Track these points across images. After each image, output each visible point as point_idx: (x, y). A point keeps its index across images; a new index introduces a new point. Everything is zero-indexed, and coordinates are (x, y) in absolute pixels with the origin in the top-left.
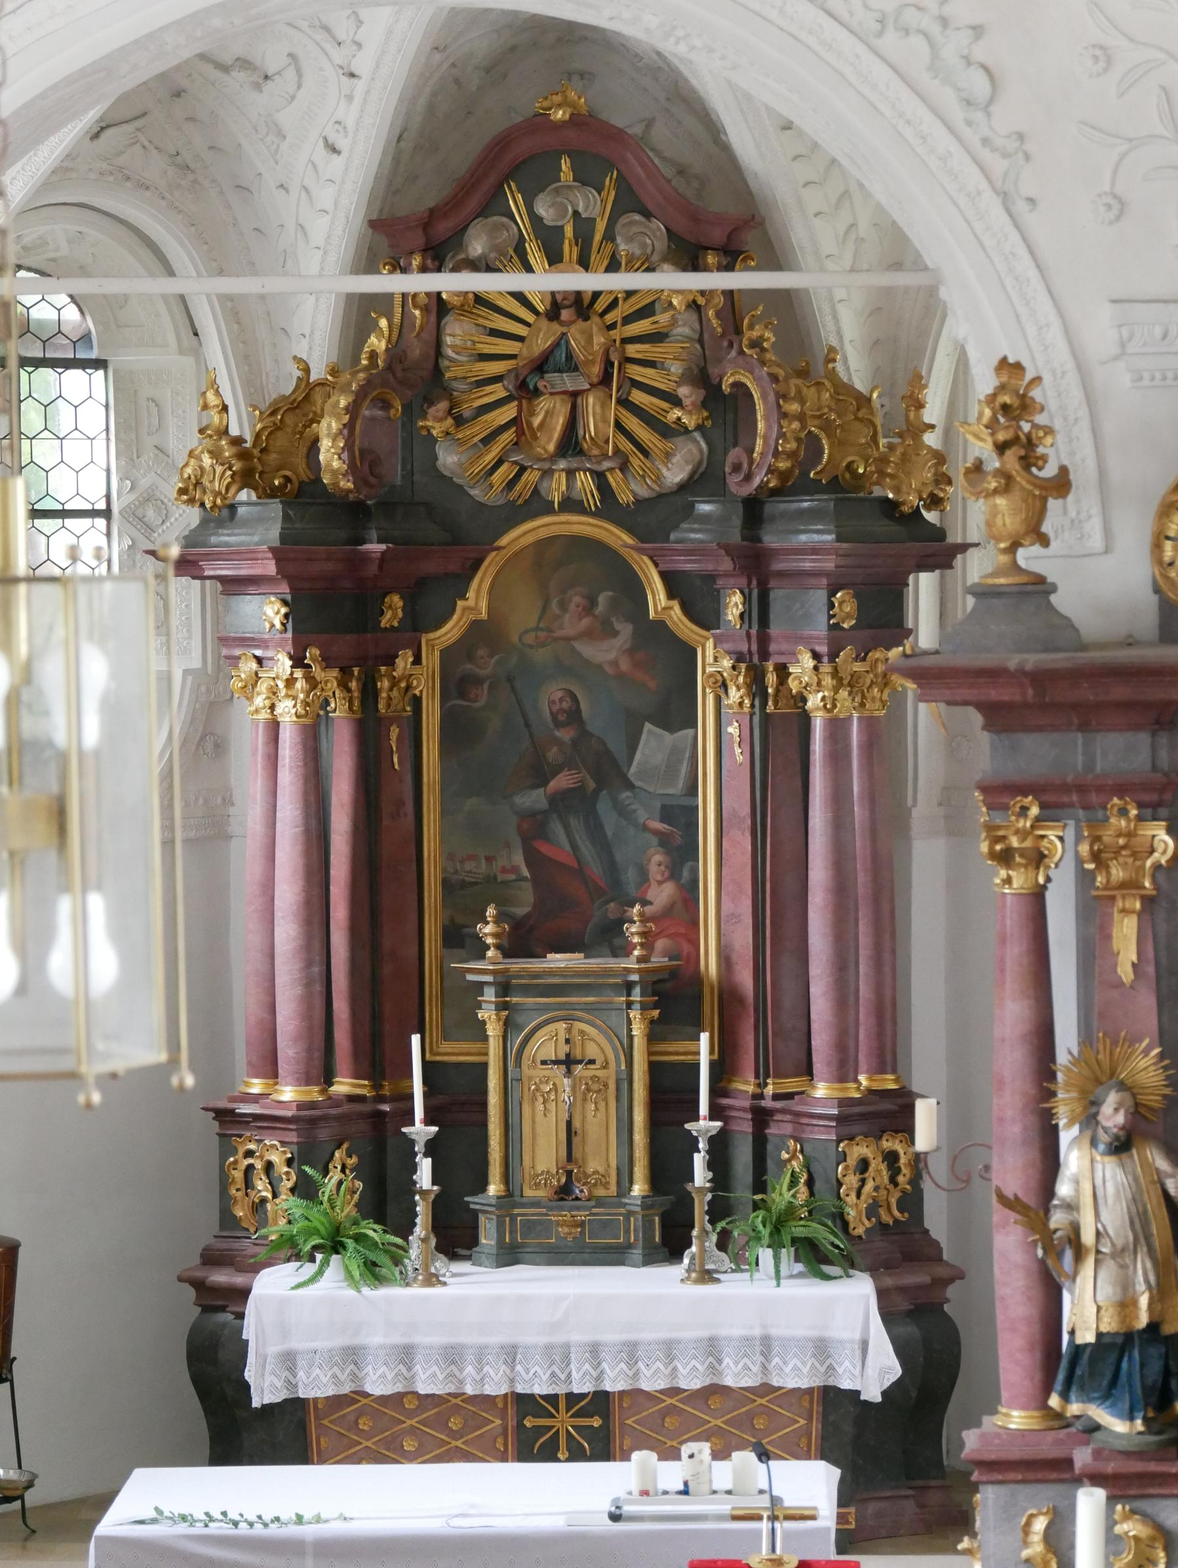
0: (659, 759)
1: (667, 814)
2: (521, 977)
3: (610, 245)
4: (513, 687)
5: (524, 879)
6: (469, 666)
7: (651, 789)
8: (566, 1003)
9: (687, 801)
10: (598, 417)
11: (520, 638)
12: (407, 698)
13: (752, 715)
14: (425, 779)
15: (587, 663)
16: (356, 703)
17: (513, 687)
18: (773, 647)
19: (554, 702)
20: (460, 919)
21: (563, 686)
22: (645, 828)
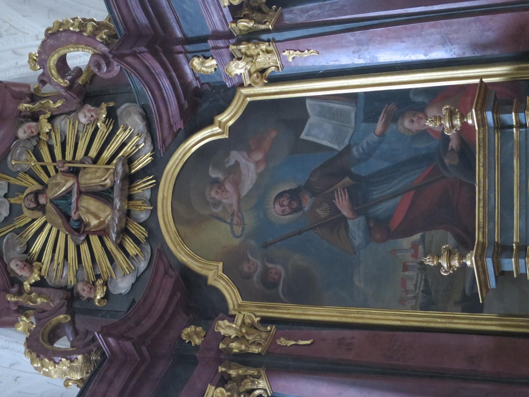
0: (328, 126)
1: (371, 117)
2: (491, 232)
3: (20, 174)
4: (271, 244)
5: (423, 237)
6: (255, 278)
7: (351, 131)
8: (520, 188)
9: (361, 102)
10: (93, 176)
11: (238, 237)
12: (262, 329)
13: (274, 41)
14: (336, 319)
15: (256, 186)
16: (251, 372)
17: (271, 244)
18: (220, 27)
19: (283, 211)
20: (457, 296)
21: (272, 203)
22: (382, 135)
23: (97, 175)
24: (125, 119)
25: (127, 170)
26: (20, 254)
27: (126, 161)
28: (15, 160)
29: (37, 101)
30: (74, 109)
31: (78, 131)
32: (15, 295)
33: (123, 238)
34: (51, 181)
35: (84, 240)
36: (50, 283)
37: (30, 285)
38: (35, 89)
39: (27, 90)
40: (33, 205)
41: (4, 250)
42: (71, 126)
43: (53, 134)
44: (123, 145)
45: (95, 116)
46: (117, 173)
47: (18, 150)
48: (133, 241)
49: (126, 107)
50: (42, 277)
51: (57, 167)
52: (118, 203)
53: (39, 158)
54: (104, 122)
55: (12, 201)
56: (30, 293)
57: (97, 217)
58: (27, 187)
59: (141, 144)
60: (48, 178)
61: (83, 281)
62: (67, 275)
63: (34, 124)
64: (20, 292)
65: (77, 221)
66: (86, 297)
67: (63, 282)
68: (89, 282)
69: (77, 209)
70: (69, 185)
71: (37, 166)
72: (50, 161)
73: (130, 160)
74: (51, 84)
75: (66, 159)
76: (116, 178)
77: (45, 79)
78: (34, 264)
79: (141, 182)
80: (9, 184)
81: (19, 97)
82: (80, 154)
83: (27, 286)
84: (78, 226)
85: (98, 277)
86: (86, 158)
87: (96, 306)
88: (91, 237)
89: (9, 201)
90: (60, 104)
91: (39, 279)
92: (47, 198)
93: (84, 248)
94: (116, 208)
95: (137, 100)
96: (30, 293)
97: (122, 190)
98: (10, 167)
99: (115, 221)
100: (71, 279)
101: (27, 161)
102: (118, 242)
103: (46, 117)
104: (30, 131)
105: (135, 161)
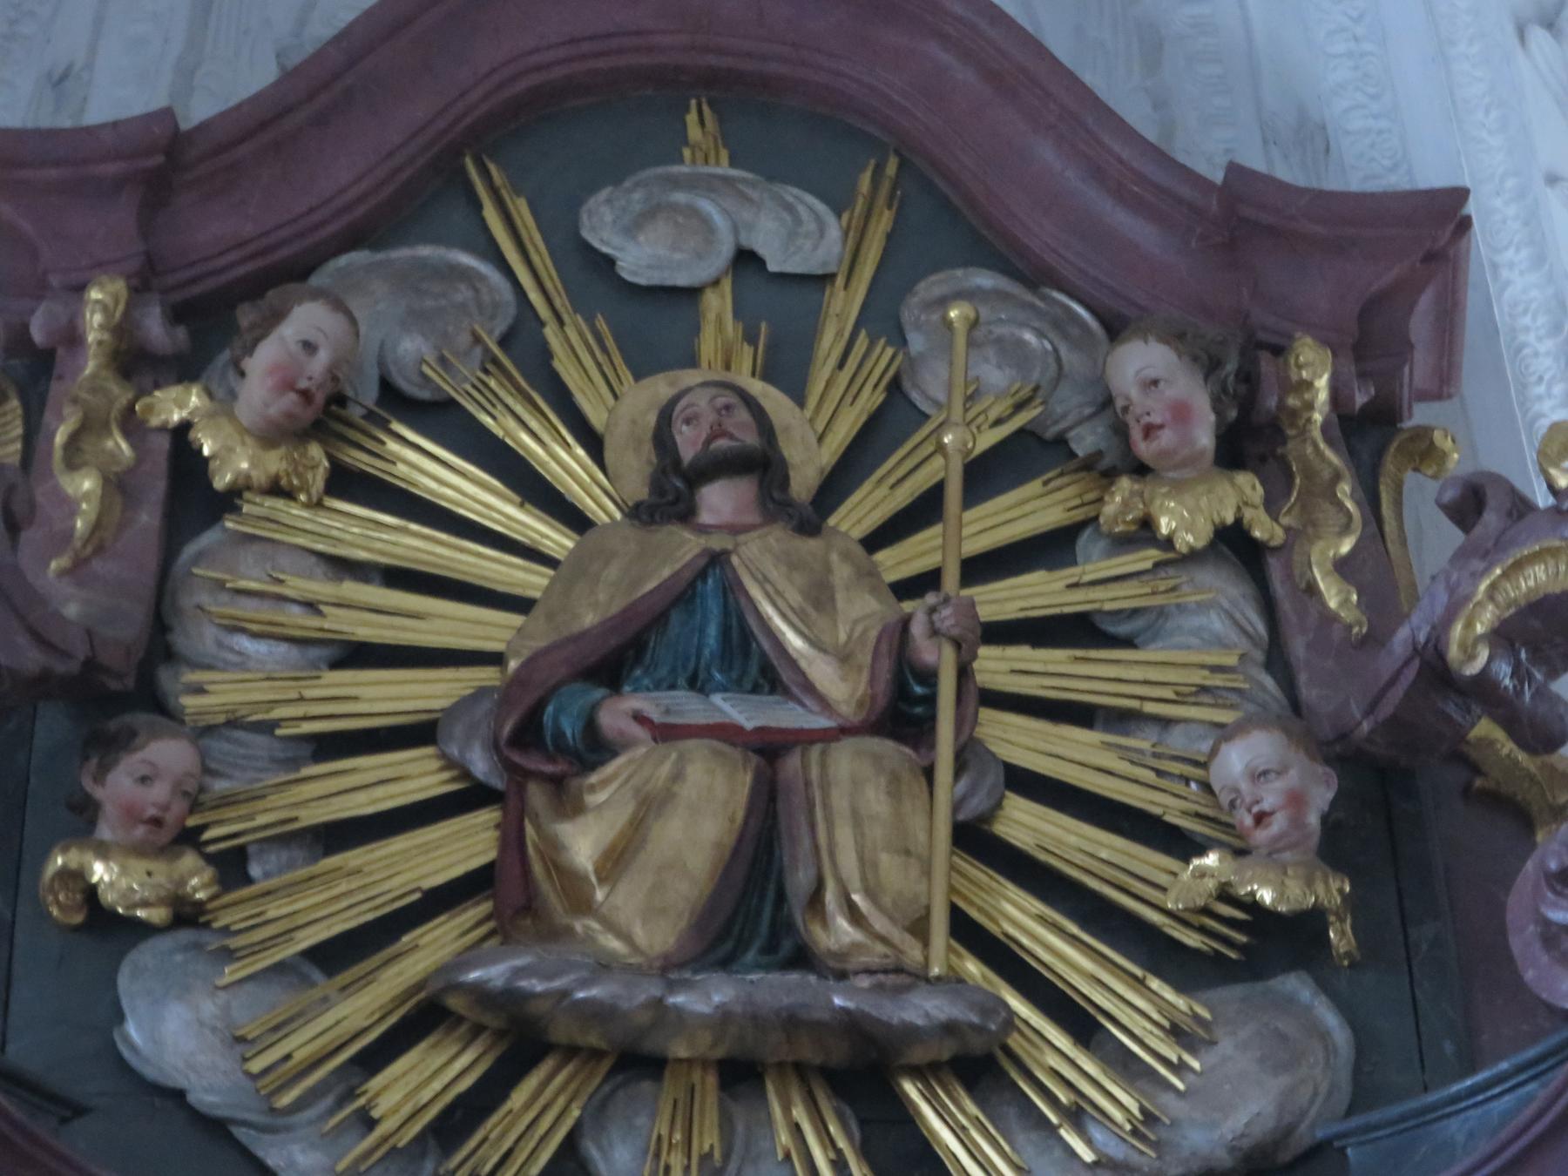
10: (876, 833)
23: (885, 859)
24: (1244, 1033)
25: (918, 1055)
26: (381, 363)
27: (977, 1045)
28: (974, 324)
29: (1352, 454)
30: (1309, 693)
31: (1166, 722)
32: (123, 330)
33: (477, 1030)
34: (846, 556)
35: (466, 774)
36: (190, 550)
37: (185, 427)
38: (1423, 433)
39: (1419, 381)
40: (688, 443)
41: (401, 253)
42: (1198, 677)
43: (1146, 558)
44: (1082, 1024)
45: (1261, 836)
46: (899, 990)
47: (1040, 334)
48: (460, 1098)
49: (1324, 1036)
50: (229, 501)
51: (931, 598)
52: (708, 996)
53: (986, 475)
54: (1225, 894)
55: (718, 305)
56: (131, 424)
57: (615, 861)
58: (800, 401)
59: (1089, 1142)
60: (858, 532)
61: (207, 771)
62: (243, 663)
63: (1205, 439)
64: (135, 363)
65: (590, 727)
66: (99, 793)
67: (199, 637)
68: (195, 807)
69: (666, 733)
70: (823, 672)
71: (938, 461)
72: (972, 547)
73: (982, 1069)
74: (1461, 555)
75: (983, 651)
76: (864, 982)
77: (1491, 519)
78: (315, 451)
79: (842, 1143)
80: (825, 279)
81: (1370, 342)
82: (1018, 740)
83: (178, 404)
84: (559, 735)
85: (232, 867)
86: (995, 777)
87: (45, 855)
88: (487, 817)
89: (716, 283)
90: (1333, 604)
91: (222, 481)
92: (735, 530)
93: (416, 775)
94: (672, 987)
95: (1375, 1116)
96: (131, 424)
97: (792, 1023)
98: (931, 287)
99: (584, 984)
100: (212, 694)
101: (970, 399)
102: (455, 1002)
103: (1248, 514)
104: (1156, 419)
105: (981, 1103)
